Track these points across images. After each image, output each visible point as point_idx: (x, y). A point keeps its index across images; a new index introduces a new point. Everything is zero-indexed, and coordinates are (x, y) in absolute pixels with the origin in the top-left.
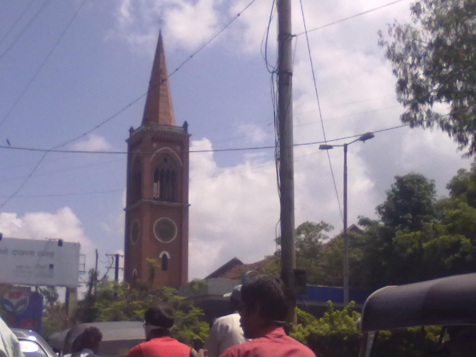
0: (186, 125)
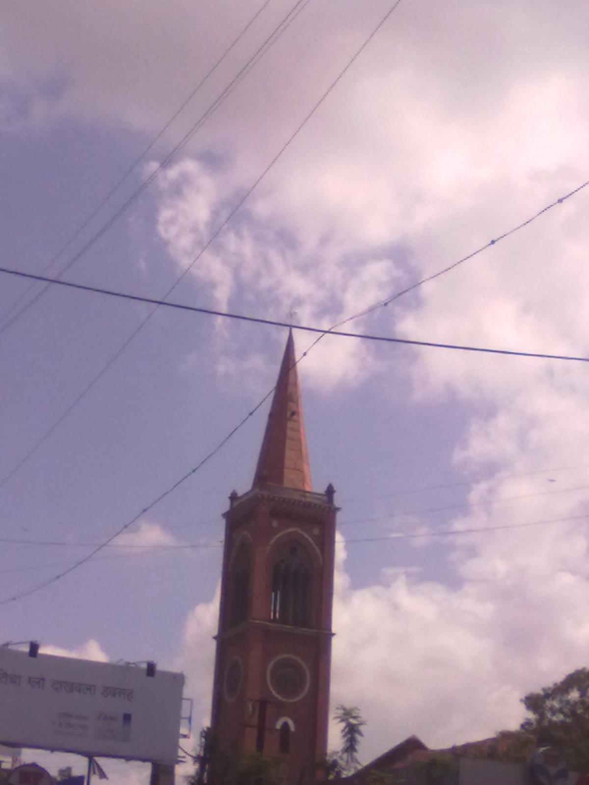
0: (330, 491)
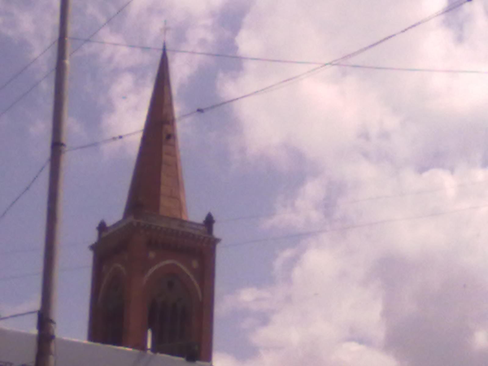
0: (209, 221)
